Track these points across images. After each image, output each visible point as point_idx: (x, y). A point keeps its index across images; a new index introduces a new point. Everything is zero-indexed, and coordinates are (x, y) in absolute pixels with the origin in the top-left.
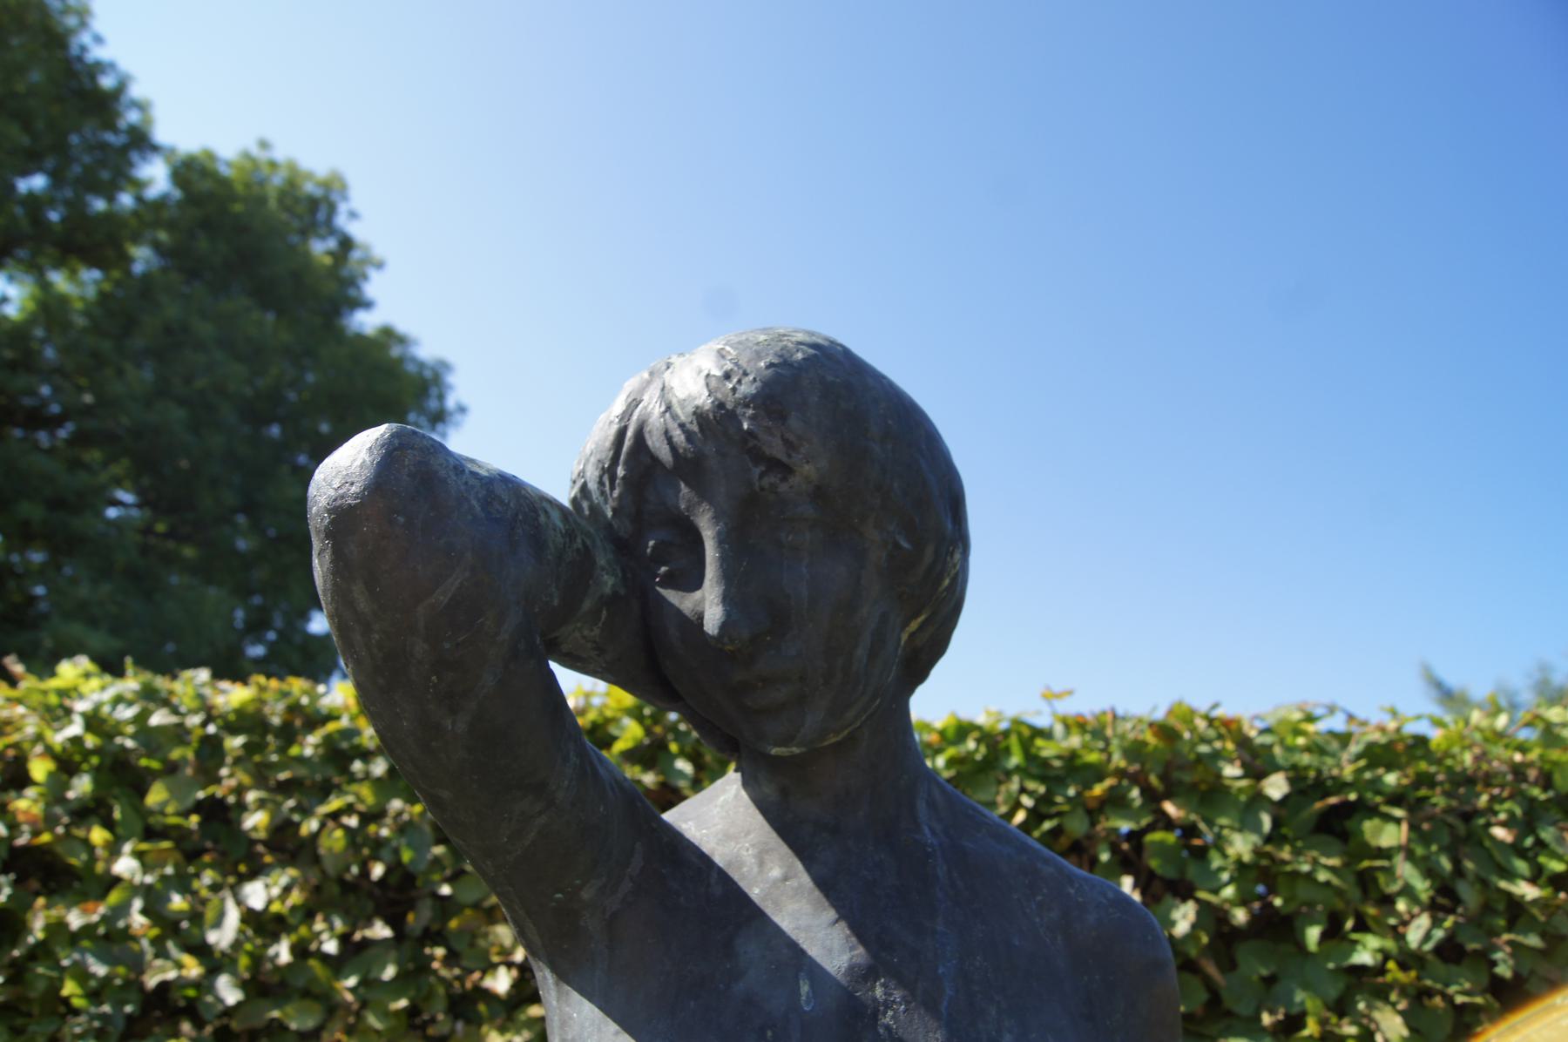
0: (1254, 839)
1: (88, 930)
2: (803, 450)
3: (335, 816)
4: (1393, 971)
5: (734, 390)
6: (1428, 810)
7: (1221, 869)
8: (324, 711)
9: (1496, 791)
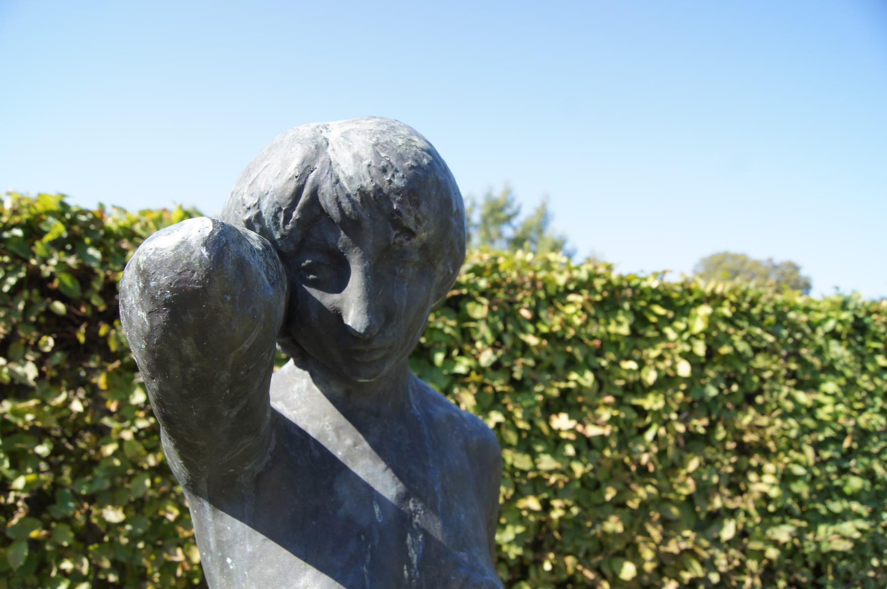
2: (424, 225)
4: (474, 376)
5: (390, 182)
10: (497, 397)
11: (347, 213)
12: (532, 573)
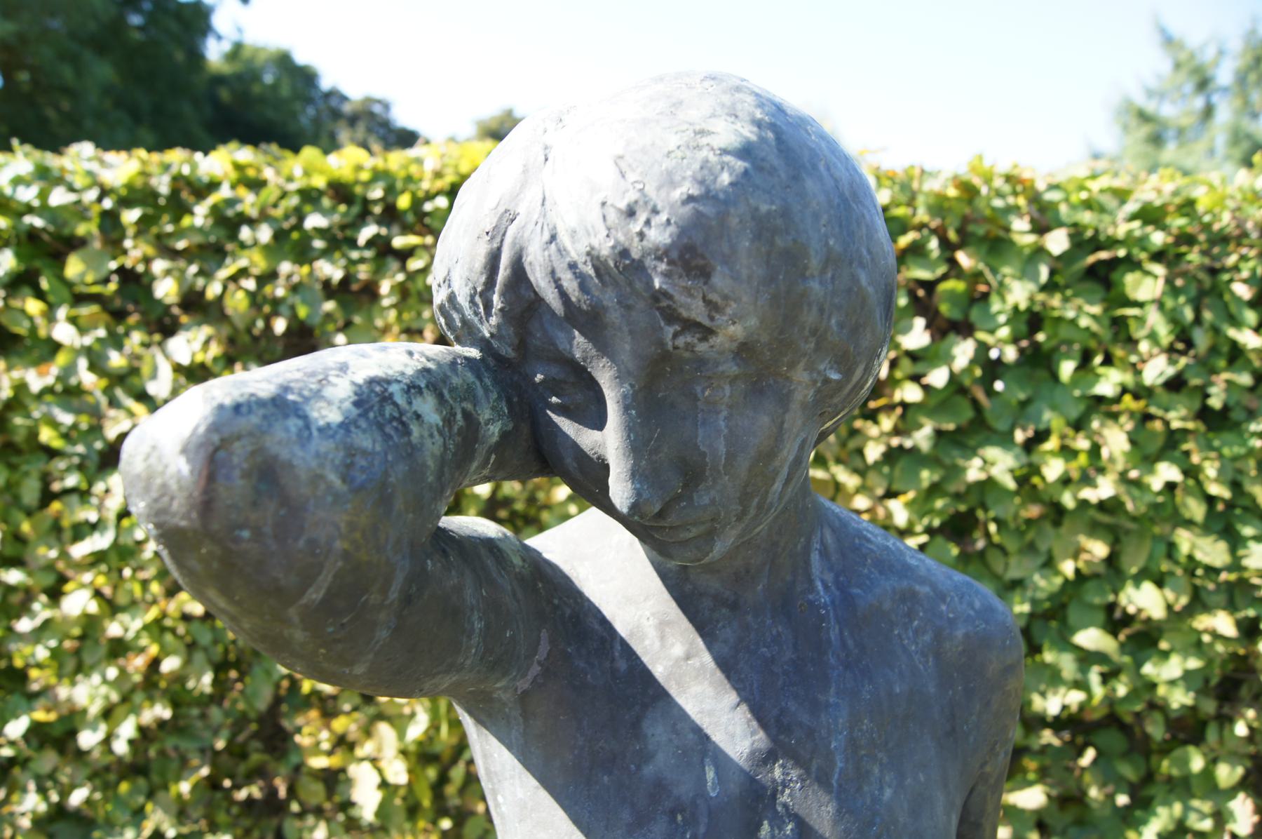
0: (1030, 287)
1: (49, 390)
2: (729, 311)
3: (234, 278)
5: (641, 235)
6: (1183, 267)
7: (999, 312)
8: (206, 179)
9: (1244, 251)
10: (1173, 439)
11: (574, 299)
12: (1212, 734)
